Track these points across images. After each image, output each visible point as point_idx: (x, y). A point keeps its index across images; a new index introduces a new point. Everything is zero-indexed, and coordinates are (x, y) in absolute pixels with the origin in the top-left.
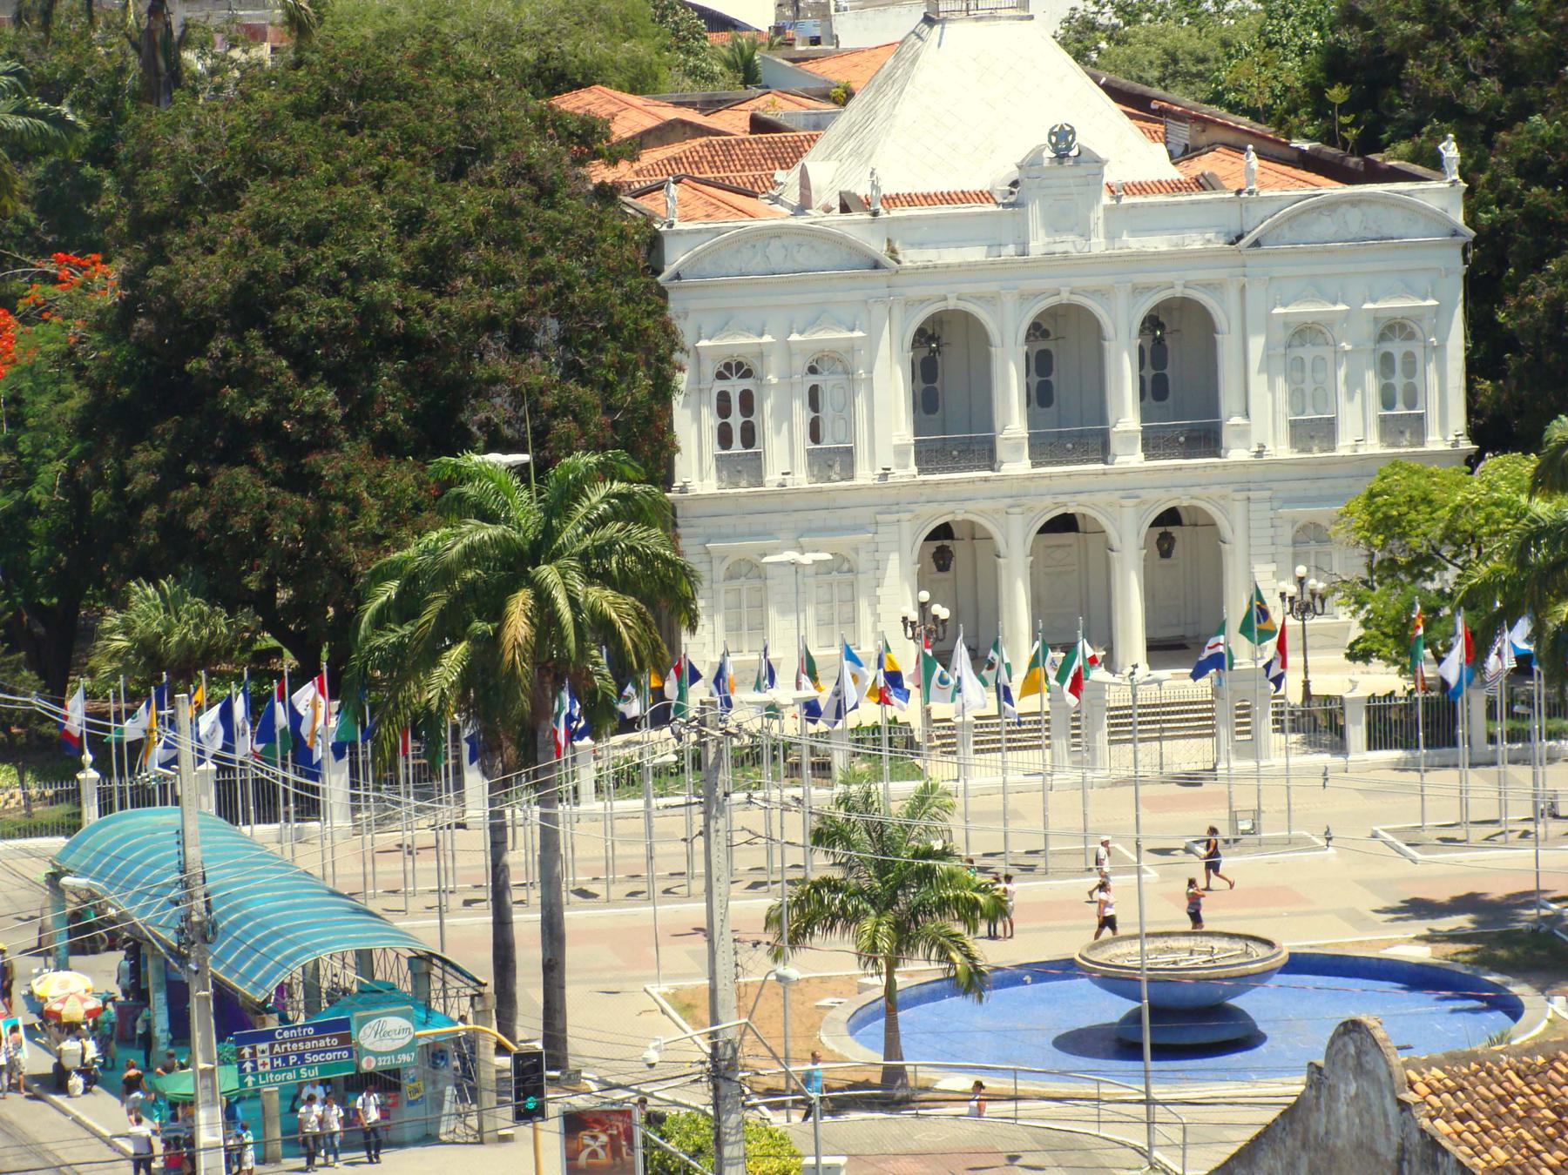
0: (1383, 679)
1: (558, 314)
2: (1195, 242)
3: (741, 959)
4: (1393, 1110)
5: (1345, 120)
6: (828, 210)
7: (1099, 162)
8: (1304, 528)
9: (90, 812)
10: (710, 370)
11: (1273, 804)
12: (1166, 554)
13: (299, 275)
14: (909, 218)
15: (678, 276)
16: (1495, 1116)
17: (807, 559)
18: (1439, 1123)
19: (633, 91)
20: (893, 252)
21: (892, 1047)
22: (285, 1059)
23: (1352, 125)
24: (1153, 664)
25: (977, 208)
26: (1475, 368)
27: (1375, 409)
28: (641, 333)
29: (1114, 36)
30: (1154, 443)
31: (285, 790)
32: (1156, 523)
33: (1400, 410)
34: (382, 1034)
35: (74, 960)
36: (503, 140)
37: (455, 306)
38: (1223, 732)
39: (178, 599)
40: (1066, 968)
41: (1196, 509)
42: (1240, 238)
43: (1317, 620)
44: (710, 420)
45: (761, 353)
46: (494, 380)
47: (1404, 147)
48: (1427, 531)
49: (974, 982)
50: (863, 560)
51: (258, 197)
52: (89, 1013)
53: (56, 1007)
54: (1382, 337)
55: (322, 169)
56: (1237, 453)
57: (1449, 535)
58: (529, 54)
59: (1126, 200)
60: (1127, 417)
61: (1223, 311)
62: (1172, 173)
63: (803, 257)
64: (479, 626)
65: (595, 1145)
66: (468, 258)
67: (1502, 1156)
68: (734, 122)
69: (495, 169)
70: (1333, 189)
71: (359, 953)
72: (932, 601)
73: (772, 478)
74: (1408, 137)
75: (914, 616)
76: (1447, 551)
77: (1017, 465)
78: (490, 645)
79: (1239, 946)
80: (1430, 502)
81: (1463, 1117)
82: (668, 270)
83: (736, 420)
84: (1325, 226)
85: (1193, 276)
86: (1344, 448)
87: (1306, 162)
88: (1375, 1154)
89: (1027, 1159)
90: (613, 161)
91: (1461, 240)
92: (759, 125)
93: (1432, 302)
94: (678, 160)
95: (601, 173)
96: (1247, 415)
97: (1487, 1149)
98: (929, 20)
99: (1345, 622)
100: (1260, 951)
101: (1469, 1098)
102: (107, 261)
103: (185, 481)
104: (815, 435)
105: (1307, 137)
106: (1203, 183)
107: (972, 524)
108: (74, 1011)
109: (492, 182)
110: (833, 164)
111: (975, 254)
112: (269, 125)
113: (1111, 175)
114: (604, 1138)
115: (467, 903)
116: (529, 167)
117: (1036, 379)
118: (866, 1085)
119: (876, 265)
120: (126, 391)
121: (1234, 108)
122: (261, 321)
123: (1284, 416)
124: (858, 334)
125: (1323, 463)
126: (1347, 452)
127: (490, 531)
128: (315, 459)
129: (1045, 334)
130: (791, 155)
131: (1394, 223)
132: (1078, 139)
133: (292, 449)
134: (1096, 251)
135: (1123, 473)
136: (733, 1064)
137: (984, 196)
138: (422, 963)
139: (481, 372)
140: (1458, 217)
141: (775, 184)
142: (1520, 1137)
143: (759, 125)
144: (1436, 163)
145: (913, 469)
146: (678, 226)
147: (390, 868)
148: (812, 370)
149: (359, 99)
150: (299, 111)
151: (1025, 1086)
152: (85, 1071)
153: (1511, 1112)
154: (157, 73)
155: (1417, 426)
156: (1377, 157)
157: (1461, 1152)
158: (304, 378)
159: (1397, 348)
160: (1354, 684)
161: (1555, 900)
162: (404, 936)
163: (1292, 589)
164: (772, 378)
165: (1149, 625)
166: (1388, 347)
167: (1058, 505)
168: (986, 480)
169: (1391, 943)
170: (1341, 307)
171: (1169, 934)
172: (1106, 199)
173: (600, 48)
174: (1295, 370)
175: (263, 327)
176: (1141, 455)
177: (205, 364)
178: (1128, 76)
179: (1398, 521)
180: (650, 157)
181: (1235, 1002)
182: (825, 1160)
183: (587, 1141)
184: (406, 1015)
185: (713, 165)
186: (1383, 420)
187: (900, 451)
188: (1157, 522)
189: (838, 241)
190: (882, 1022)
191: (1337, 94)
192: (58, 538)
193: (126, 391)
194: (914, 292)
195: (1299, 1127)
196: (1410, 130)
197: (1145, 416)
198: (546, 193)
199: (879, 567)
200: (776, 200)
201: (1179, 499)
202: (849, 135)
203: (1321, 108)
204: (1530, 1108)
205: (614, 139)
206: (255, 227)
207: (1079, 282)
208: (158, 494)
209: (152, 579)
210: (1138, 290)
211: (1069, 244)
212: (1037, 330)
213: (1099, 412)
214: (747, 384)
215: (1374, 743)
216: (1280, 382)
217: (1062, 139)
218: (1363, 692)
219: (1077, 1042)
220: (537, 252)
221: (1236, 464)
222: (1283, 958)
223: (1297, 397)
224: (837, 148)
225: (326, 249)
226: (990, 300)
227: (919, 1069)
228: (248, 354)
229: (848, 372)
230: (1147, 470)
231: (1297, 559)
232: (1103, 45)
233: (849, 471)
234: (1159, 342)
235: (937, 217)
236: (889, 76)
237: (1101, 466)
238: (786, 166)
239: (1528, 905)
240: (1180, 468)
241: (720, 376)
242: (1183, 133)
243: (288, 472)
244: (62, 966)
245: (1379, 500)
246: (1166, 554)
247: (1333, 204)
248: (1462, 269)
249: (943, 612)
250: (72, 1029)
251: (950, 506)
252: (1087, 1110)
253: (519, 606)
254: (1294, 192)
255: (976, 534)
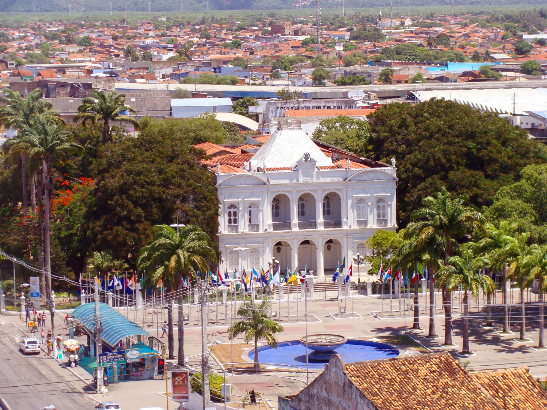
0: (375, 278)
1: (193, 193)
2: (336, 180)
3: (209, 338)
4: (343, 375)
5: (372, 153)
6: (255, 171)
7: (315, 161)
8: (360, 244)
9: (83, 303)
10: (227, 206)
11: (349, 306)
12: (329, 249)
13: (135, 183)
14: (272, 173)
15: (220, 185)
16: (365, 376)
17: (243, 249)
18: (353, 378)
19: (216, 144)
20: (268, 181)
21: (256, 359)
22: (110, 360)
23: (374, 154)
24: (325, 274)
25: (288, 171)
26: (399, 209)
27: (376, 218)
28: (211, 199)
29: (325, 133)
30: (326, 225)
31: (117, 300)
32: (326, 243)
33: (382, 218)
34: (132, 355)
35: (75, 337)
36: (182, 154)
37: (170, 192)
38: (340, 289)
39: (105, 256)
40: (297, 342)
41: (336, 240)
42: (346, 179)
43: (362, 265)
44: (227, 217)
45: (238, 203)
46: (177, 208)
47: (384, 159)
48: (386, 245)
49: (274, 345)
50: (260, 250)
51: (126, 165)
52: (77, 349)
53: (69, 347)
54: (378, 202)
55: (140, 159)
56: (345, 227)
57: (391, 247)
58: (192, 135)
59: (321, 170)
60: (321, 219)
61: (342, 196)
62: (332, 164)
63: (248, 182)
64: (166, 263)
65: (179, 380)
66: (173, 181)
67: (366, 385)
68: (237, 151)
69: (179, 161)
70: (368, 169)
71: (138, 336)
72: (275, 259)
73: (240, 231)
74: (386, 157)
75: (271, 262)
76: (391, 250)
77: (296, 229)
78: (167, 267)
79: (337, 338)
80: (387, 239)
81: (358, 377)
82: (218, 184)
83: (232, 218)
84: (365, 177)
85: (336, 187)
86: (369, 226)
87: (364, 163)
88: (339, 385)
89: (280, 385)
90: (207, 160)
91: (395, 181)
92: (243, 152)
93: (389, 194)
94: (223, 159)
95: (203, 162)
96: (347, 219)
97: (363, 384)
98: (278, 129)
99: (368, 265)
100: (341, 339)
101: (360, 372)
102: (93, 180)
103: (107, 230)
104: (250, 222)
105: (363, 156)
106: (338, 167)
107: (286, 242)
108: (73, 348)
109: (179, 164)
110: (257, 161)
111: (287, 181)
112: (128, 149)
113: (318, 165)
114: (181, 379)
115: (149, 326)
116: (187, 161)
117: (275, 211)
118: (251, 368)
119: (265, 184)
120: (95, 209)
121: (350, 150)
122: (126, 193)
123: (356, 219)
124: (260, 199)
125: (364, 230)
126: (370, 227)
127: (168, 241)
128: (137, 225)
129: (303, 200)
130: (248, 159)
131: (381, 176)
132: (311, 156)
133: (132, 222)
134: (314, 181)
135: (319, 231)
136: (207, 363)
137: (289, 169)
138: (151, 339)
139: (175, 206)
140: (395, 175)
141: (244, 165)
142: (370, 382)
143: (243, 152)
144: (391, 164)
145: (272, 229)
146: (220, 174)
147: (149, 317)
148: (250, 207)
149: (149, 144)
150: (135, 146)
151: (281, 368)
152: (75, 362)
153: (369, 376)
154: (106, 138)
155: (386, 221)
156: (378, 162)
157: (357, 385)
158: (135, 207)
159: (381, 204)
160: (369, 279)
161: (409, 329)
162: (147, 333)
163: (356, 258)
164: (241, 209)
165: (324, 266)
166: (379, 204)
167: (304, 238)
168: (288, 232)
169: (372, 338)
170: (369, 195)
171: (321, 335)
172: (316, 170)
173: (208, 134)
174: (358, 208)
175: (126, 195)
176: (298, 228)
177: (112, 202)
178: (327, 143)
179: (380, 243)
180: (215, 159)
181: (334, 350)
182: (226, 384)
183: (177, 379)
184: (138, 350)
185: (231, 161)
186: (378, 221)
187: (269, 225)
188: (277, 244)
189: (256, 178)
190: (254, 355)
191: (370, 147)
192: (80, 241)
193: (95, 209)
194: (272, 190)
195: (323, 378)
196: (387, 156)
197: (325, 218)
198: (191, 167)
199: (264, 251)
200: (244, 168)
201: (332, 237)
202: (260, 154)
203: (367, 151)
204: (373, 375)
205: (207, 154)
206: (125, 172)
207: (310, 188)
208: (101, 233)
209: (99, 251)
210: (323, 190)
211: (308, 180)
212: (301, 199)
213: (314, 217)
214: (235, 210)
215: (373, 293)
216: (355, 211)
217: (307, 156)
218: (371, 281)
219: (301, 359)
220: (188, 180)
221: (344, 230)
222: (346, 340)
223: (358, 215)
224: (258, 157)
225: (142, 177)
226: (290, 192)
227: (262, 365)
228: (122, 200)
229: (258, 207)
230: (325, 231)
231: (358, 251)
232: (324, 135)
233: (258, 230)
234: (328, 202)
235: (279, 173)
236: (269, 141)
237: (314, 230)
238: (247, 161)
239: (403, 330)
240: (332, 230)
241: (229, 208)
242: (336, 156)
243: (131, 228)
244: (72, 338)
245: (376, 238)
246: (329, 249)
247: (367, 172)
248: (396, 187)
249: (277, 262)
250: (72, 352)
251: (280, 238)
252: (295, 374)
253: (173, 258)
254: (358, 169)
255: (286, 244)
